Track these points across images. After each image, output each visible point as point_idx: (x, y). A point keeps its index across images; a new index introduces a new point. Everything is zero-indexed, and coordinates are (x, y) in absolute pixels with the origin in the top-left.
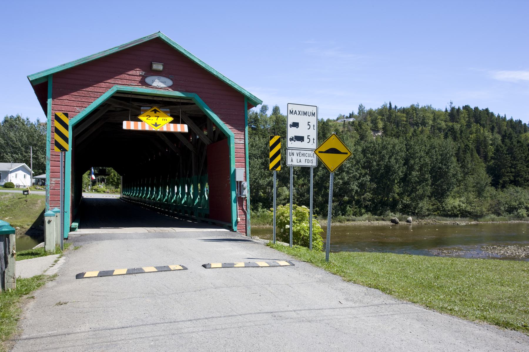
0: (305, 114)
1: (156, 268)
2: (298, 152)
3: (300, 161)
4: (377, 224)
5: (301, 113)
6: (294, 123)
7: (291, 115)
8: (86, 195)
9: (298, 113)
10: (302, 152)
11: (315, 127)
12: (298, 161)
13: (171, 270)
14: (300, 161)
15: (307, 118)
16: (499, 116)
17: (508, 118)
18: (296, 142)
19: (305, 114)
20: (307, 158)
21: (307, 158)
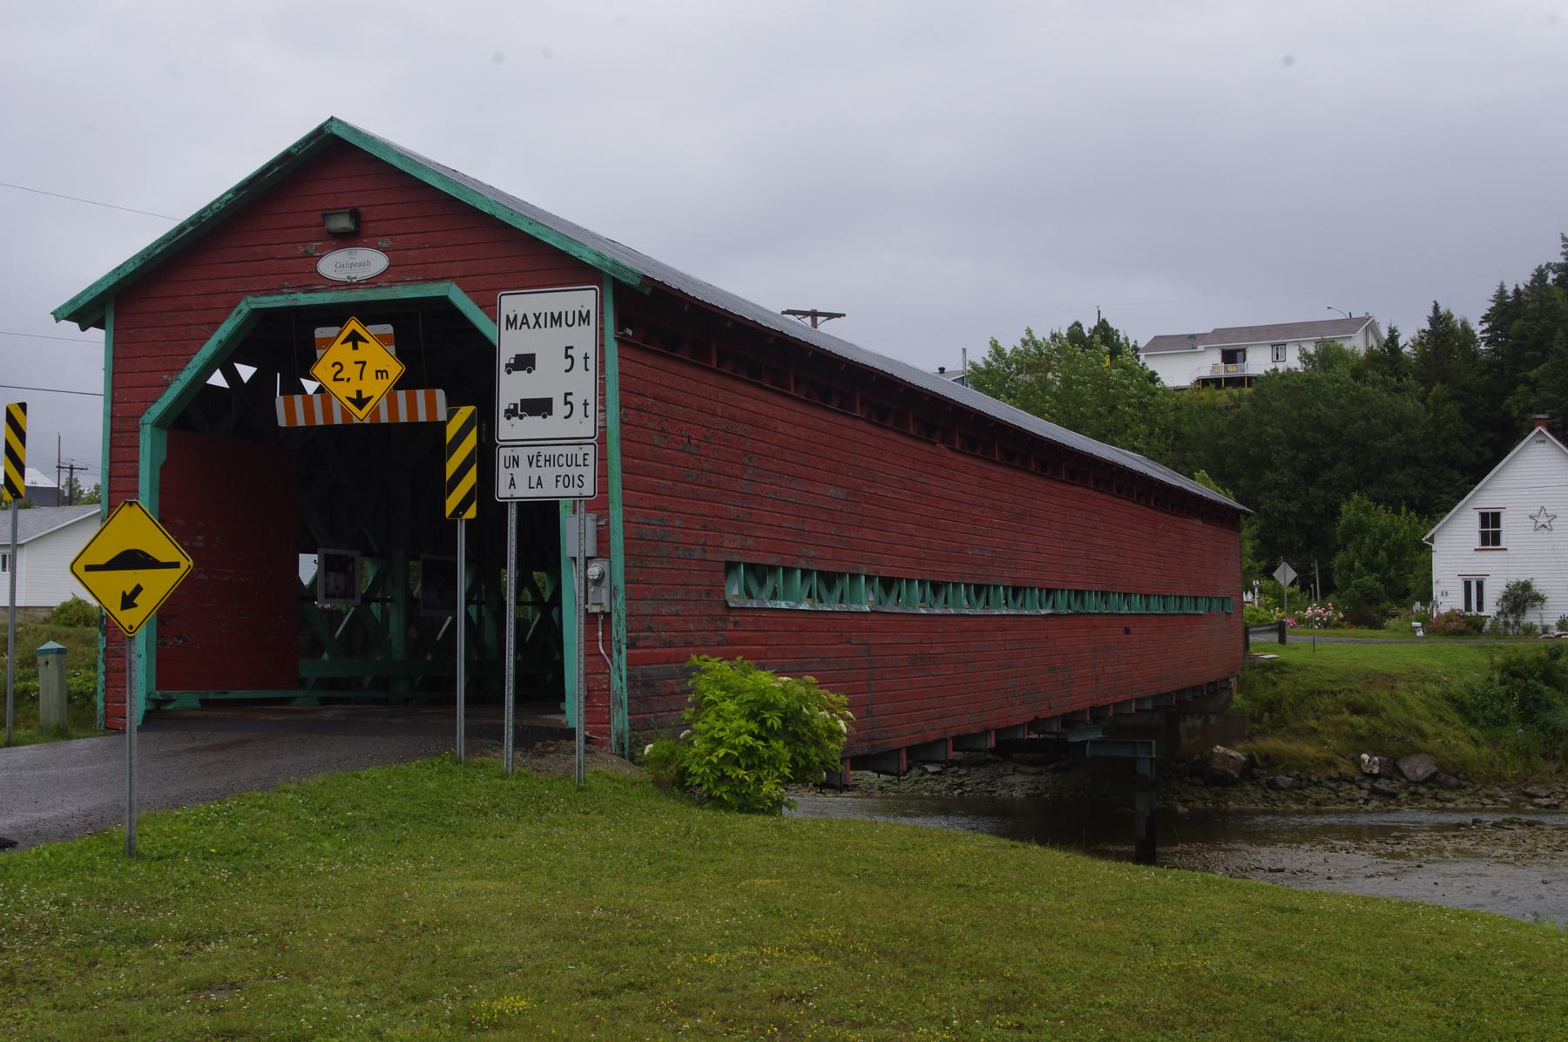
0: (556, 320)
3: (540, 483)
5: (542, 320)
6: (518, 357)
9: (532, 321)
12: (534, 484)
14: (540, 483)
15: (562, 335)
18: (527, 419)
19: (556, 320)
20: (564, 471)
21: (564, 471)
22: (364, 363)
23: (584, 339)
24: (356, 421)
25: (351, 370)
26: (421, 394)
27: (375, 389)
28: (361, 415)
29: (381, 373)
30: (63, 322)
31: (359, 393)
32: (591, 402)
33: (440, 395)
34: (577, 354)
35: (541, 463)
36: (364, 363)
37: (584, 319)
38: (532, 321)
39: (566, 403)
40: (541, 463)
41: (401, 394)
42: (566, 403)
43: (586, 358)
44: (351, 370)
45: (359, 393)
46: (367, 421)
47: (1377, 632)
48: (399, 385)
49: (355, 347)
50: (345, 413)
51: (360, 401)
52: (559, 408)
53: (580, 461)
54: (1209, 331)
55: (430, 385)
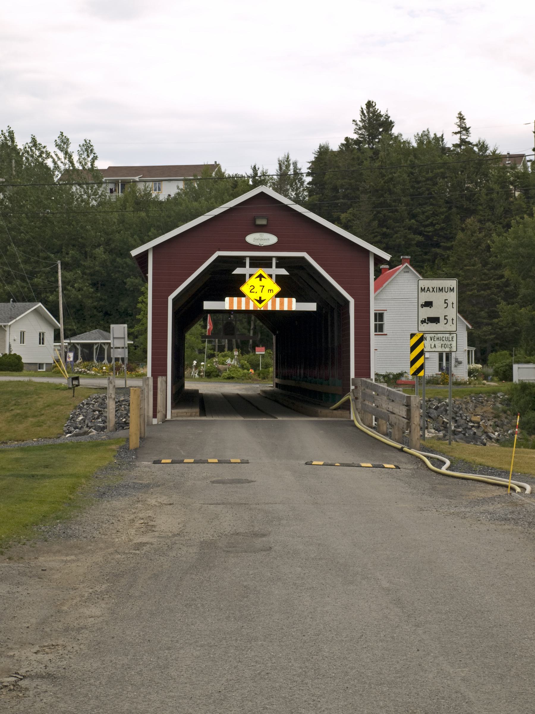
0: (441, 290)
1: (395, 466)
2: (433, 335)
3: (435, 346)
4: (415, 416)
5: (435, 290)
6: (426, 302)
7: (423, 293)
8: (189, 385)
9: (431, 290)
10: (439, 335)
11: (455, 305)
12: (433, 346)
13: (208, 463)
14: (435, 346)
15: (443, 295)
16: (309, 168)
17: (304, 161)
18: (430, 324)
19: (441, 290)
20: (445, 342)
21: (445, 342)
22: (264, 286)
23: (453, 297)
24: (259, 309)
25: (258, 289)
26: (286, 300)
27: (267, 296)
28: (260, 307)
29: (270, 291)
30: (424, 308)
31: (260, 298)
32: (455, 319)
33: (294, 300)
34: (449, 302)
35: (435, 340)
36: (264, 286)
37: (452, 290)
38: (431, 290)
39: (445, 319)
40: (435, 340)
41: (278, 300)
42: (445, 319)
43: (453, 304)
44: (258, 289)
45: (260, 298)
46: (262, 309)
47: (264, 389)
48: (277, 296)
49: (261, 280)
50: (255, 305)
51: (260, 301)
52: (442, 319)
53: (450, 339)
54: (106, 168)
55: (289, 296)
